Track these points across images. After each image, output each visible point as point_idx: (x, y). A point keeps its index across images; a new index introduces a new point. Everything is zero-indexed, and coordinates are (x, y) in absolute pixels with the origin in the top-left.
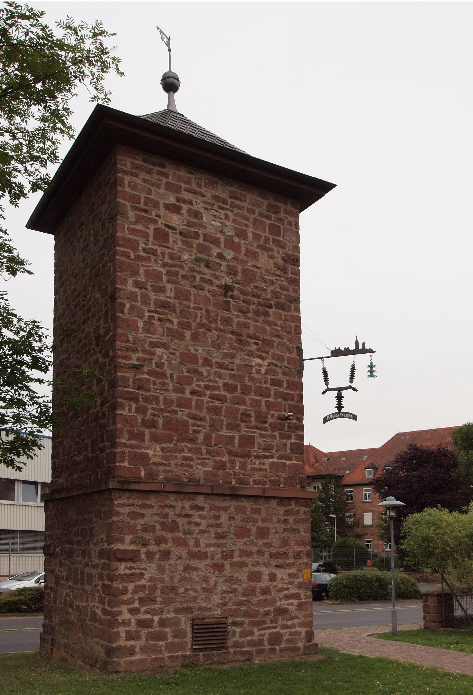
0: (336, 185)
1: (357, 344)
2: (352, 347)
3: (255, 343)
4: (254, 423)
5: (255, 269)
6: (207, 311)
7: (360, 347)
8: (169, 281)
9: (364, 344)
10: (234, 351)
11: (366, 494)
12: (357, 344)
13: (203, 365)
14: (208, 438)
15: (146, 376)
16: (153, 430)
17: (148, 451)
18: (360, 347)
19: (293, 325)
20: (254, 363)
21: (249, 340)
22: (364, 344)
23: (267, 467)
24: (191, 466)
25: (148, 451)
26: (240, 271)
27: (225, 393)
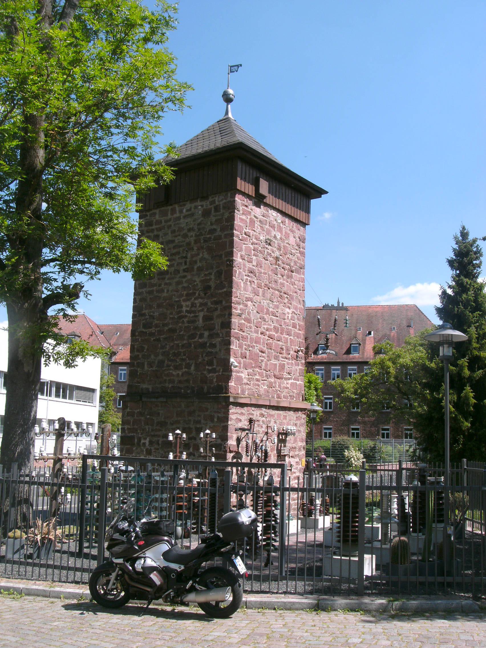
0: (326, 192)
1: (338, 303)
2: (336, 305)
3: (287, 298)
4: (284, 355)
5: (288, 245)
6: (269, 275)
7: (341, 305)
8: (254, 255)
9: (343, 304)
10: (278, 303)
11: (121, 374)
12: (338, 303)
13: (266, 314)
14: (266, 365)
15: (243, 322)
16: (245, 359)
17: (242, 375)
18: (341, 305)
19: (302, 284)
20: (286, 312)
21: (284, 295)
22: (343, 304)
23: (289, 386)
24: (259, 385)
25: (242, 375)
26: (282, 247)
27: (274, 334)
